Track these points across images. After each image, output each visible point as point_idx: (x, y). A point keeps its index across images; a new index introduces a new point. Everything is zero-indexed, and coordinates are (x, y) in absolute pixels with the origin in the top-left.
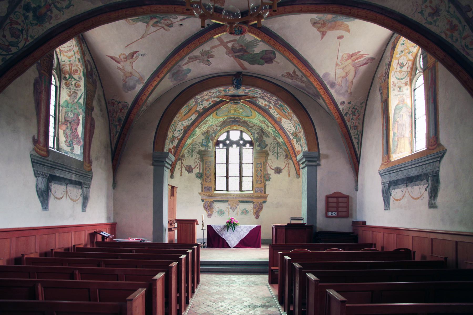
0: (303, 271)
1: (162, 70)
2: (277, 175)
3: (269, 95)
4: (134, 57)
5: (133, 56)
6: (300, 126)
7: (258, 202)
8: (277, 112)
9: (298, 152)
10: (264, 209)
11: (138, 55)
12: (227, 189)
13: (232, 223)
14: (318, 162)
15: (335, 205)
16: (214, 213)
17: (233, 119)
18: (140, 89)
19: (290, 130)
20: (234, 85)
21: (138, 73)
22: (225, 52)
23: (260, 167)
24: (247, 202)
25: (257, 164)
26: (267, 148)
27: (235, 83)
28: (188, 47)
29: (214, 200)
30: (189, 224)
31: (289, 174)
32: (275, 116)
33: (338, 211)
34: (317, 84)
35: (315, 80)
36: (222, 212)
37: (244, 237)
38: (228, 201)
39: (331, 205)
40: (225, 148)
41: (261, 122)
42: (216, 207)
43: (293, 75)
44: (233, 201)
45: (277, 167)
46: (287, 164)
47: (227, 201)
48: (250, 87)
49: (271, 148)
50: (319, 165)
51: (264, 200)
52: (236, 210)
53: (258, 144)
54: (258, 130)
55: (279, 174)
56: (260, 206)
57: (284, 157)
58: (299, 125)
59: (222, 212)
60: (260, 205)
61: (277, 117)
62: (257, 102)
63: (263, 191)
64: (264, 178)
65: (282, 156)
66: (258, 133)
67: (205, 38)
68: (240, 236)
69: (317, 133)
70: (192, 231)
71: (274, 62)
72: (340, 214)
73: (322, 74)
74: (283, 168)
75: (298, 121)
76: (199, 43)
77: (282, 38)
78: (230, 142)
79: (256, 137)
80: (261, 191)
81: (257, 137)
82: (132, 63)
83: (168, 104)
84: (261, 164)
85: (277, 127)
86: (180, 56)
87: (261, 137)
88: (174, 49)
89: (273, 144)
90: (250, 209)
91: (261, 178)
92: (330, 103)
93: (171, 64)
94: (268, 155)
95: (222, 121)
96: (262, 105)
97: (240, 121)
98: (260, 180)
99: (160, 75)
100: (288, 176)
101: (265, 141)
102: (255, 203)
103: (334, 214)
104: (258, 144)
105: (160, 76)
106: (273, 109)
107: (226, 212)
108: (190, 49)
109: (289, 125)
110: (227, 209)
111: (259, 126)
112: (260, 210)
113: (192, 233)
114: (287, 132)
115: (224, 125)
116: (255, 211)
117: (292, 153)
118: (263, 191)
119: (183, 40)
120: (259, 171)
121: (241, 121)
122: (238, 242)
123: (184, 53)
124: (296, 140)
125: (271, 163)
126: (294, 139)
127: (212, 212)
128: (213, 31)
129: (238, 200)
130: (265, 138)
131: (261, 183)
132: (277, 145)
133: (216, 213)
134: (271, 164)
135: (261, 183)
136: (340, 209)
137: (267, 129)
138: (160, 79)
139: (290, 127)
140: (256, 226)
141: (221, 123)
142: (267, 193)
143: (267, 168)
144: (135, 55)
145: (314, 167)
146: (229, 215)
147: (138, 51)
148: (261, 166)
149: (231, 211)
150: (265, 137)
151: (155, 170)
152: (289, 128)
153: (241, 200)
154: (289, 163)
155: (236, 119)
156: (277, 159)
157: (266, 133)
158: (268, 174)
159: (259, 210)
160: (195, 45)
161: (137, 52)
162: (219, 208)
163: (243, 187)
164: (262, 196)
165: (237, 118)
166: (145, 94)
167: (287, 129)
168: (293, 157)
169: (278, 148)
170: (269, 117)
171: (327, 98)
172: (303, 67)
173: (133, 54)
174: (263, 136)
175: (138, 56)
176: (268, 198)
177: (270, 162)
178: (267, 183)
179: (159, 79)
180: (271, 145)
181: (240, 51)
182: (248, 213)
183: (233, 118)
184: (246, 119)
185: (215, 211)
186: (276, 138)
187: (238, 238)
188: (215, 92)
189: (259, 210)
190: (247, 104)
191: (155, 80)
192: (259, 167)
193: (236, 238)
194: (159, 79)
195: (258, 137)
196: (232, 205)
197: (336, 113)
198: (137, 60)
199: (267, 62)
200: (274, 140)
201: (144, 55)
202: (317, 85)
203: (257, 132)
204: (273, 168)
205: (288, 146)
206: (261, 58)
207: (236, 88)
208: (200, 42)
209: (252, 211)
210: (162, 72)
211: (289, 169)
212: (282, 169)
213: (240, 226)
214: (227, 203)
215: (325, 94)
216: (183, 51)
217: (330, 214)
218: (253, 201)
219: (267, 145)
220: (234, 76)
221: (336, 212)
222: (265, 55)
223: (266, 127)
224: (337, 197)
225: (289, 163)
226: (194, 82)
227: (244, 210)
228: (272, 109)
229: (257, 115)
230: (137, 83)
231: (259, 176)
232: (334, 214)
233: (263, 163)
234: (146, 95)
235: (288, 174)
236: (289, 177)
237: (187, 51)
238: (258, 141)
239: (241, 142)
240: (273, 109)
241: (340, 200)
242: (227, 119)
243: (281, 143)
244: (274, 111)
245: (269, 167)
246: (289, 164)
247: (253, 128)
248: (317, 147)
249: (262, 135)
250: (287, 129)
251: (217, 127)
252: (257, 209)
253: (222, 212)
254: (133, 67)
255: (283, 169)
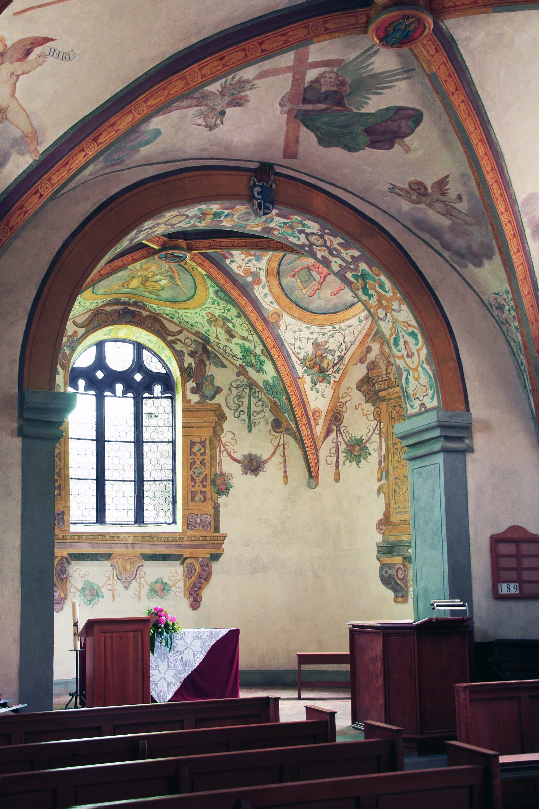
0: (504, 759)
1: (112, 120)
2: (250, 477)
3: (340, 240)
4: (32, 56)
5: (28, 53)
6: (420, 337)
7: (197, 559)
8: (274, 297)
9: (313, 414)
10: (215, 579)
11: (48, 52)
12: (101, 519)
13: (163, 626)
14: (467, 441)
15: (512, 563)
16: (70, 596)
17: (122, 307)
18: (21, 171)
19: (299, 351)
20: (255, 201)
21: (28, 117)
22: (283, 95)
23: (201, 454)
24: (165, 557)
25: (193, 444)
26: (219, 399)
27: (256, 195)
28: (221, 59)
29: (70, 555)
30: (131, 634)
31: (286, 477)
32: (266, 306)
33: (520, 581)
34: (510, 222)
35: (506, 210)
36: (95, 592)
37: (195, 666)
38: (110, 555)
39: (505, 562)
40: (93, 392)
41: (212, 320)
42: (76, 575)
43: (430, 191)
44: (126, 555)
45: (250, 455)
46: (278, 445)
47: (108, 557)
48: (290, 210)
49: (230, 400)
50: (471, 450)
51: (214, 551)
52: (134, 585)
53: (194, 385)
54: (193, 345)
55: (256, 475)
56: (204, 570)
57: (270, 427)
58: (413, 334)
59: (93, 590)
60: (202, 566)
61: (271, 309)
62: (228, 261)
63: (210, 524)
64: (212, 485)
65: (262, 423)
66: (192, 354)
67: (285, 38)
68: (184, 664)
69: (463, 360)
70: (140, 656)
71: (396, 145)
72: (528, 589)
73: (524, 196)
74: (268, 456)
75: (413, 322)
76: (262, 51)
77: (473, 76)
78: (138, 372)
79: (186, 365)
80: (204, 524)
81: (190, 364)
82: (18, 76)
83: (66, 234)
84: (203, 443)
85: (268, 339)
86: (187, 84)
87: (201, 364)
88: (167, 56)
89: (237, 388)
90: (173, 579)
91: (204, 486)
92: (525, 278)
93: (149, 103)
94: (222, 417)
95: (91, 310)
96: (237, 271)
97: (139, 314)
98: (201, 492)
99: (104, 134)
100: (281, 480)
101: (212, 377)
102: (187, 561)
103: (512, 589)
104: (194, 385)
105: (102, 139)
106: (263, 287)
107: (106, 592)
108: (224, 66)
109: (297, 335)
110: (109, 582)
111: (197, 334)
112: (202, 581)
113: (140, 663)
114: (289, 355)
115: (95, 323)
116: (189, 584)
117: (300, 414)
118: (210, 524)
119: (208, 32)
120: (195, 466)
121: (145, 313)
122: (177, 686)
123: (203, 76)
124: (312, 378)
125: (233, 442)
126: (305, 376)
127: (66, 593)
128: (319, 20)
129: (139, 551)
130: (212, 370)
131: (205, 500)
132: (247, 390)
133: (78, 594)
134: (231, 447)
135: (205, 500)
136: (526, 575)
137: (223, 342)
138: (102, 147)
139: (300, 340)
140: (225, 631)
141: (87, 315)
142: (222, 530)
143: (220, 456)
144: (37, 51)
145: (460, 456)
146: (114, 600)
147: (52, 40)
148: (203, 450)
149: (119, 586)
150: (212, 366)
151: (25, 453)
152: (298, 343)
153: (148, 551)
154: (284, 444)
155: (130, 308)
156: (250, 431)
157: (216, 356)
158: (222, 474)
159: (201, 583)
160: (246, 56)
161: (46, 40)
162: (85, 579)
163: (146, 514)
164: (208, 538)
165: (135, 304)
166: (37, 191)
167: (292, 347)
168: (304, 427)
169: (252, 399)
170: (252, 309)
171: (522, 264)
172: (492, 170)
173: (32, 44)
174: (207, 363)
175: (45, 57)
176: (226, 546)
177: (231, 441)
178: (221, 500)
179: (97, 148)
180: (230, 389)
181: (325, 97)
182: (168, 591)
183: (124, 303)
184: (165, 310)
185: (73, 589)
186: (249, 369)
187: (179, 672)
188: (190, 215)
189: (201, 583)
190: (200, 265)
191: (83, 150)
192: (198, 453)
193: (171, 673)
194: (97, 148)
195: (194, 366)
196: (121, 569)
197: (532, 306)
198: (39, 68)
199: (373, 145)
200: (238, 374)
201: (65, 57)
202: (509, 225)
203: (190, 349)
204: (239, 456)
205: (291, 393)
206: (365, 131)
207: (260, 209)
208: (264, 46)
209: (181, 584)
210: (114, 124)
211: (285, 460)
212: (266, 462)
213: (184, 633)
214: (107, 563)
215: (518, 251)
216: (200, 69)
217: (504, 589)
218: (182, 555)
219: (218, 390)
220: (251, 174)
221: (517, 584)
222: (386, 121)
223: (223, 336)
224: (517, 542)
225: (284, 444)
226: (143, 177)
227: (156, 582)
228: (260, 286)
229: (210, 300)
230: (14, 150)
231: (198, 480)
232: (512, 589)
233: (208, 443)
234: (41, 196)
235: (282, 475)
236: (286, 484)
237: (214, 70)
238: (192, 377)
239: (138, 377)
240: (263, 287)
241: (525, 548)
242: (107, 304)
243: (261, 385)
244: (266, 290)
245: (225, 454)
246: (286, 446)
247: (178, 337)
248: (463, 399)
249: (205, 359)
250: (292, 347)
251: (76, 328)
252: (194, 578)
253: (95, 592)
254: (17, 91)
255: (269, 459)
